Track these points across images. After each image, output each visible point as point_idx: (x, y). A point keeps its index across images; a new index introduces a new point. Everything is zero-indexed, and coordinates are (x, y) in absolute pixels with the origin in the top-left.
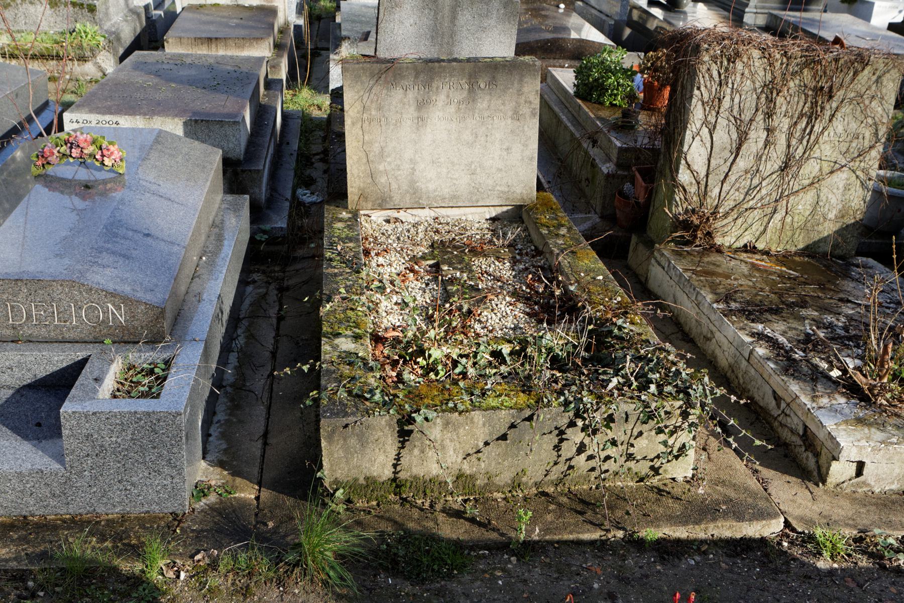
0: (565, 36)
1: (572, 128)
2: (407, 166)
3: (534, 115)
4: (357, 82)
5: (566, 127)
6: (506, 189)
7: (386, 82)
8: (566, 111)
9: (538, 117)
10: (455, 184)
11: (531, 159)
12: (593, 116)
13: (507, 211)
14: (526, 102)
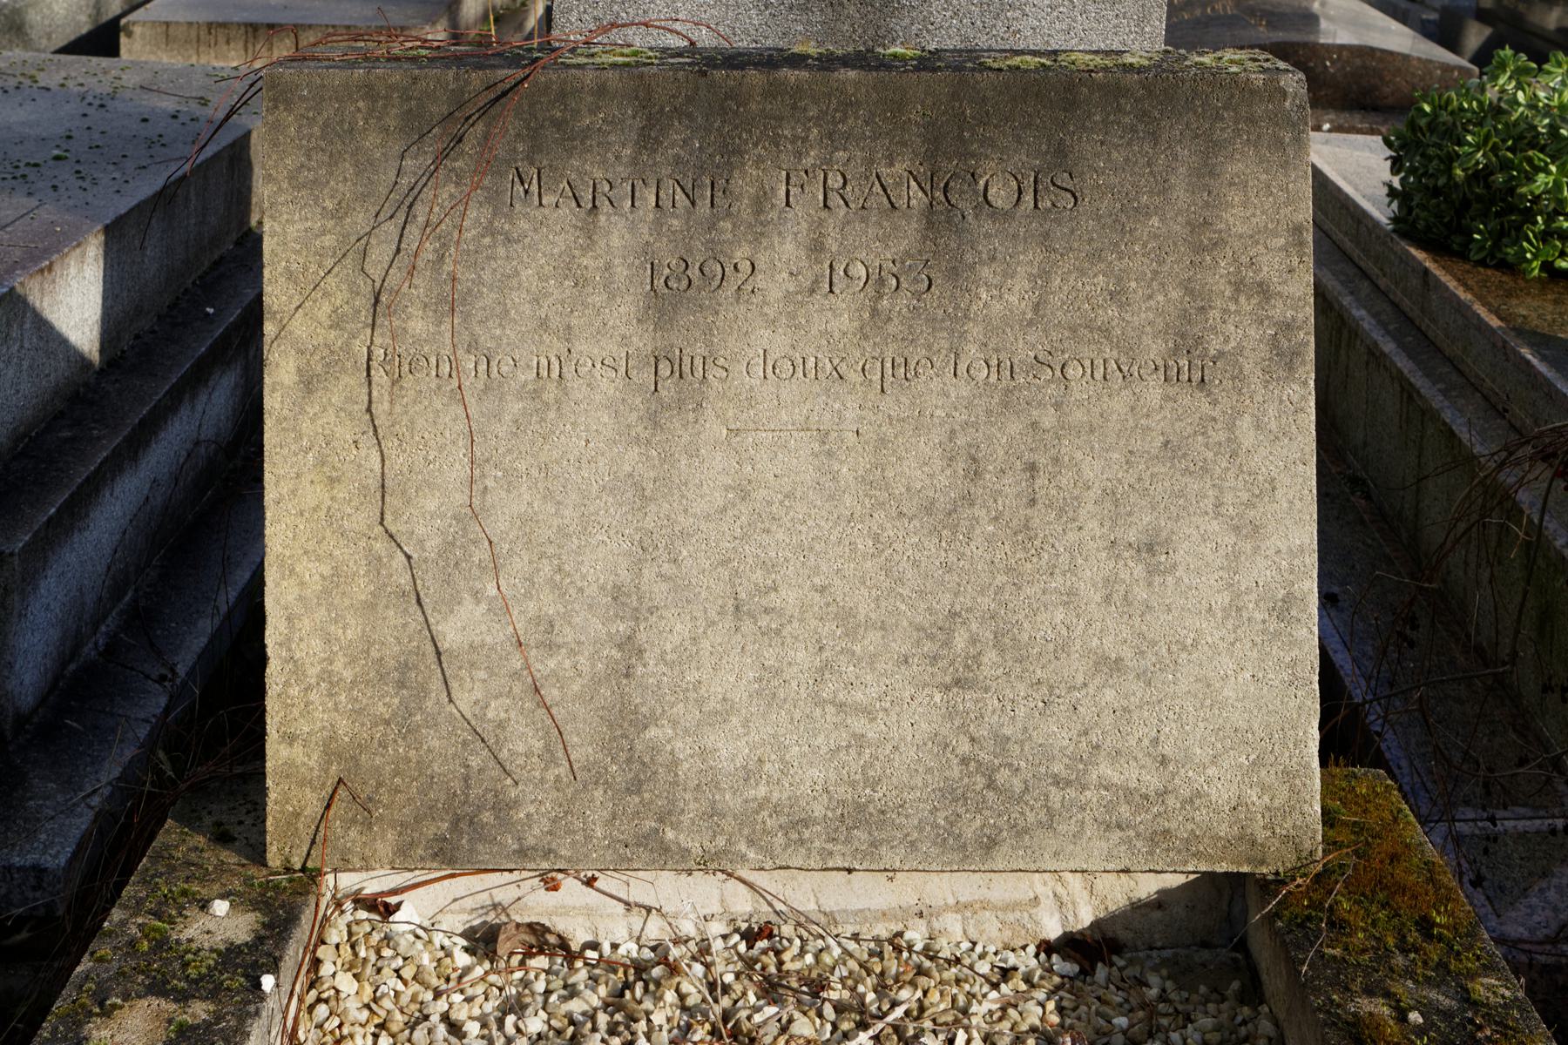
0: (1312, 38)
1: (1403, 363)
2: (597, 627)
3: (1286, 359)
4: (334, 160)
5: (1375, 355)
6: (1153, 781)
7: (487, 165)
8: (1365, 286)
9: (1307, 372)
10: (859, 740)
11: (1283, 609)
12: (1495, 322)
13: (1162, 901)
14: (1238, 286)
